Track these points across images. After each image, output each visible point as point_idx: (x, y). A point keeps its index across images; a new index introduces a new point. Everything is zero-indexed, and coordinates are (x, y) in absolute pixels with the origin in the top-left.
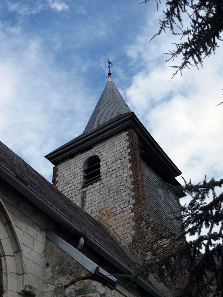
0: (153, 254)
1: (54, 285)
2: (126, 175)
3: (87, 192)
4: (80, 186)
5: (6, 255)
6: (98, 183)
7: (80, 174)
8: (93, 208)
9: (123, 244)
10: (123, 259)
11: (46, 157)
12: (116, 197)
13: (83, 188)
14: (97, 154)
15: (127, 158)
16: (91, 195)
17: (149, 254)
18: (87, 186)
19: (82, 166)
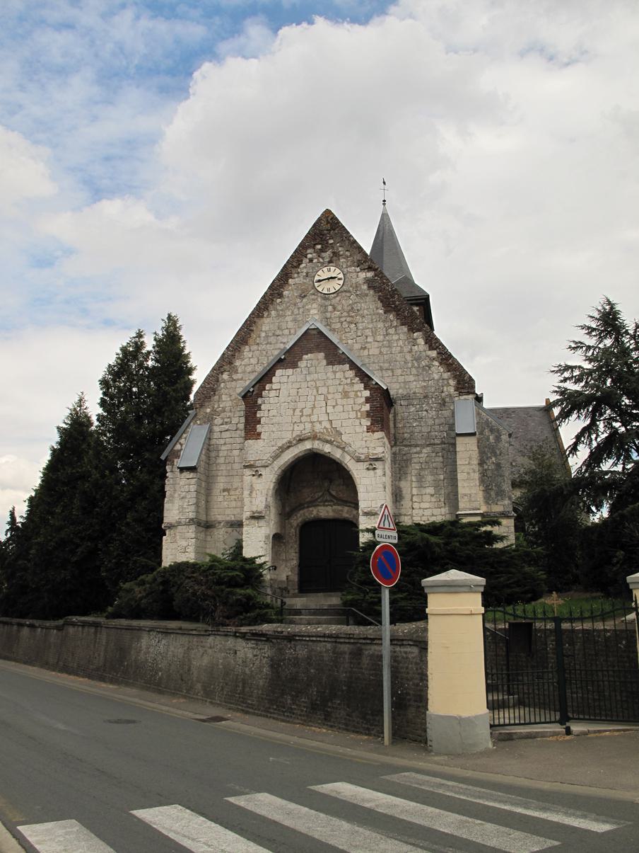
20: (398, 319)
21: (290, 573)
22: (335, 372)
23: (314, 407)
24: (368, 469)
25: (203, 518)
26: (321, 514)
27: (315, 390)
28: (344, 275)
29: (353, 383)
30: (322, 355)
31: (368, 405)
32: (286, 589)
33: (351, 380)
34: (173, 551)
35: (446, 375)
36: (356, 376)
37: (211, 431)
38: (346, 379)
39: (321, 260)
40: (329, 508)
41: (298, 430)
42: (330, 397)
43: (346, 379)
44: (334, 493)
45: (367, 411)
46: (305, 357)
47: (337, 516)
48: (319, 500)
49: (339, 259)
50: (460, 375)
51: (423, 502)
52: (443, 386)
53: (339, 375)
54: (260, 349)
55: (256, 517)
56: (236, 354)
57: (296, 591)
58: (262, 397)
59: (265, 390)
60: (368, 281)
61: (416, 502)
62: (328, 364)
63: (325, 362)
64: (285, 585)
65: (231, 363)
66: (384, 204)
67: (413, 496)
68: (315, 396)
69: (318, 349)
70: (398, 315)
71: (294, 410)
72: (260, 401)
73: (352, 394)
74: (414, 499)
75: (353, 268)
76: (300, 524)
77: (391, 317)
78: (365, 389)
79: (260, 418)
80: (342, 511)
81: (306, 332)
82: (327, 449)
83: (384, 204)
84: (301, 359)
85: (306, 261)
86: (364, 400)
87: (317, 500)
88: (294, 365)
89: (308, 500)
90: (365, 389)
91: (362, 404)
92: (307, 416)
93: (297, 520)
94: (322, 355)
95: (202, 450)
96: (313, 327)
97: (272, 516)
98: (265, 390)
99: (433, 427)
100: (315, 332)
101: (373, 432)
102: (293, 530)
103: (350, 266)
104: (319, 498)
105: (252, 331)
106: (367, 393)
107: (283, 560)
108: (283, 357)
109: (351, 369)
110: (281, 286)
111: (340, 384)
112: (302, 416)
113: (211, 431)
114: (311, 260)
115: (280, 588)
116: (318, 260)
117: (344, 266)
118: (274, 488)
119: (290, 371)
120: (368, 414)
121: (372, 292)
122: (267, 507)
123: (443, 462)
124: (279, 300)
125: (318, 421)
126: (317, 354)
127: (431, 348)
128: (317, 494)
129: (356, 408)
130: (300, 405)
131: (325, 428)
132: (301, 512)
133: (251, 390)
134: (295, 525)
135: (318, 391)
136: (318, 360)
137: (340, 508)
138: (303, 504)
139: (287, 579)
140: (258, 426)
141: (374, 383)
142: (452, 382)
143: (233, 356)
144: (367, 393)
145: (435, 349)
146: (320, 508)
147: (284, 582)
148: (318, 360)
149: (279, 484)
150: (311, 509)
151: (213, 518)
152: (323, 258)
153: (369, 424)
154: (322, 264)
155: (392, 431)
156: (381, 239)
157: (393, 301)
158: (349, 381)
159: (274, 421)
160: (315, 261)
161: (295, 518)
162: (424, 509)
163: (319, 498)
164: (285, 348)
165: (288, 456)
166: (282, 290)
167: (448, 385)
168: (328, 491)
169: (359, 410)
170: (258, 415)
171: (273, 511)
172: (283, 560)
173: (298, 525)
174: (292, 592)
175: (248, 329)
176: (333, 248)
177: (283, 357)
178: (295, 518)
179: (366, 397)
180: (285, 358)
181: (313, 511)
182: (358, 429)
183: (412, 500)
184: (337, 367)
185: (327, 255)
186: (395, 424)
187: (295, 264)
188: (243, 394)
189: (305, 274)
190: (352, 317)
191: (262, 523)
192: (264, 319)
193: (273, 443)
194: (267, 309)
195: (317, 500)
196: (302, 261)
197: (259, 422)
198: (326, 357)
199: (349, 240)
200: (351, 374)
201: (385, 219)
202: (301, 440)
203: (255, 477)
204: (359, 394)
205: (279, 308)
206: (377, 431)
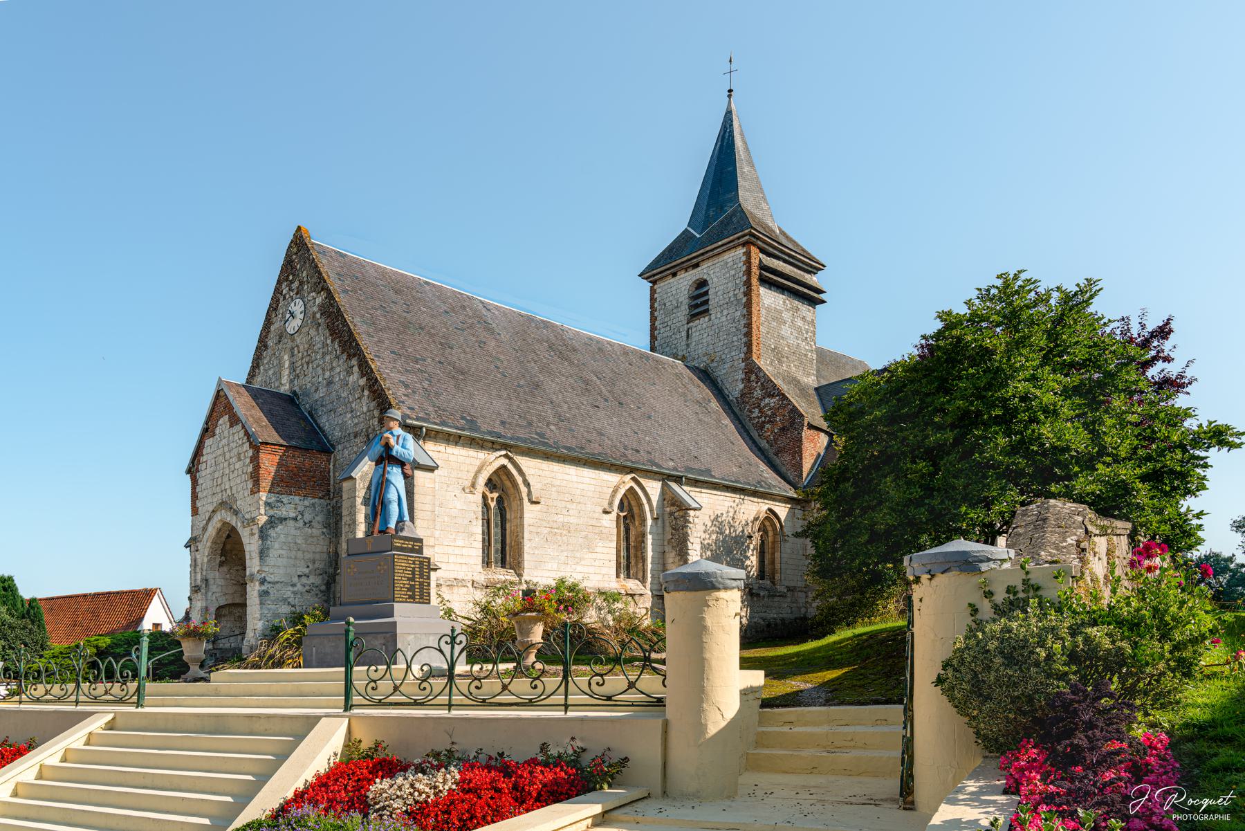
0: (760, 411)
1: (653, 349)
2: (738, 313)
3: (694, 330)
4: (684, 319)
5: (636, 686)
6: (707, 318)
7: (684, 303)
8: (700, 351)
9: (731, 398)
10: (777, 673)
11: (640, 276)
12: (726, 341)
13: (688, 323)
14: (705, 277)
15: (742, 290)
16: (698, 333)
17: (757, 410)
18: (693, 321)
19: (686, 292)
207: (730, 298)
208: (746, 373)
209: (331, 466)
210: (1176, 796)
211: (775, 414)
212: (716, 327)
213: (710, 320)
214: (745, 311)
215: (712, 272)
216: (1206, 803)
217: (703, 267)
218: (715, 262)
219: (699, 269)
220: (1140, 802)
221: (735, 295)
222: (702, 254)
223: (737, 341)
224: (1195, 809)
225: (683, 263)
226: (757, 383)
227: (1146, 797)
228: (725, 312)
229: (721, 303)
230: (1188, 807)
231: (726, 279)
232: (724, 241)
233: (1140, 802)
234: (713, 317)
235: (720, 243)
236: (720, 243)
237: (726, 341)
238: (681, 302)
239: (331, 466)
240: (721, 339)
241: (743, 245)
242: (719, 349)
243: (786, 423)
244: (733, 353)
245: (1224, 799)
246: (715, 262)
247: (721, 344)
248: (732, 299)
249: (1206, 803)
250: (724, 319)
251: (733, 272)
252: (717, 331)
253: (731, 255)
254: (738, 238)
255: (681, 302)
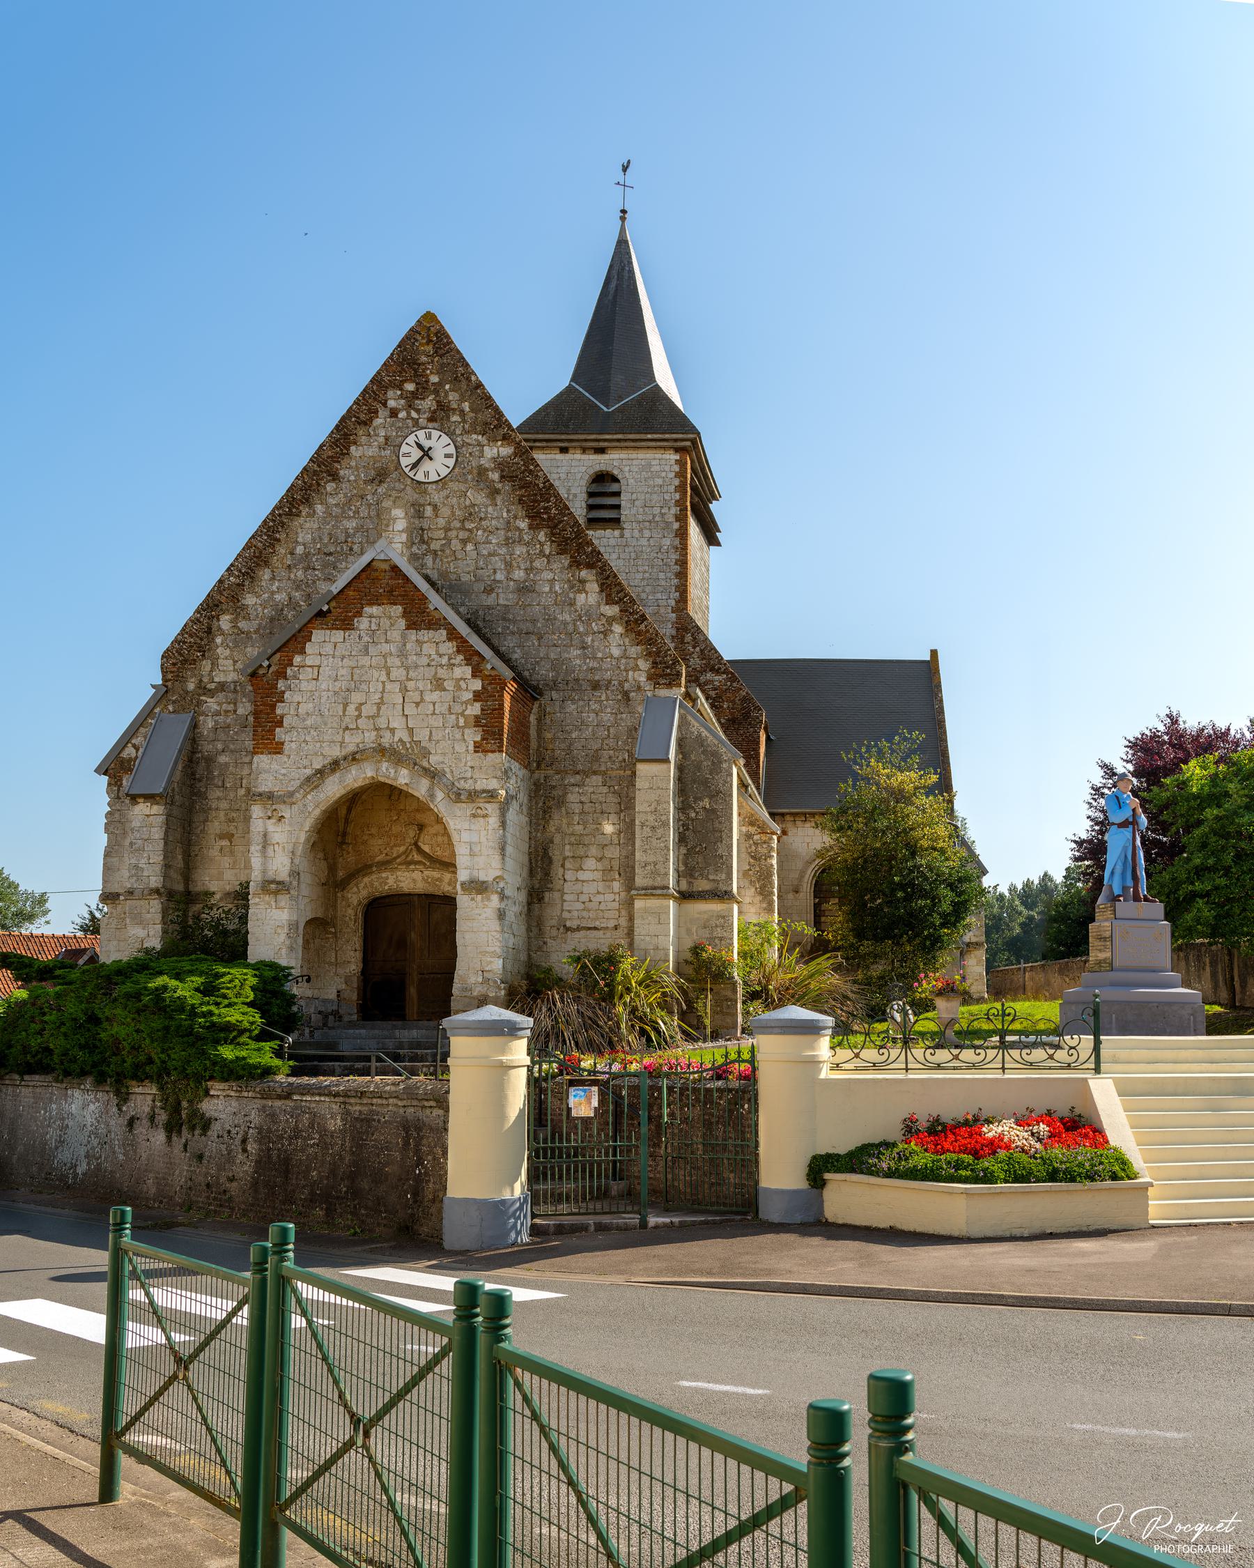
6: (617, 533)
12: (647, 575)
20: (553, 541)
21: (344, 986)
22: (420, 643)
23: (379, 705)
24: (474, 816)
25: (180, 887)
26: (402, 885)
27: (384, 673)
28: (456, 447)
29: (454, 665)
30: (399, 609)
31: (478, 705)
32: (336, 1014)
33: (450, 659)
34: (122, 944)
35: (634, 651)
36: (458, 651)
37: (194, 726)
38: (441, 656)
39: (414, 415)
40: (417, 875)
41: (352, 742)
42: (411, 685)
43: (441, 656)
44: (426, 848)
45: (476, 717)
46: (368, 610)
47: (431, 890)
48: (398, 860)
49: (448, 418)
50: (658, 653)
51: (582, 869)
52: (627, 671)
53: (429, 649)
54: (292, 576)
55: (274, 887)
56: (247, 583)
57: (355, 1017)
58: (285, 678)
59: (292, 665)
60: (500, 464)
61: (569, 870)
62: (408, 628)
63: (402, 623)
64: (330, 1008)
65: (235, 599)
66: (623, 219)
67: (565, 859)
68: (383, 683)
69: (391, 597)
70: (553, 534)
71: (345, 706)
72: (281, 685)
73: (449, 685)
74: (568, 865)
75: (474, 436)
76: (365, 902)
77: (542, 536)
78: (474, 676)
79: (282, 717)
80: (440, 880)
81: (369, 565)
82: (402, 777)
83: (623, 219)
84: (359, 614)
85: (383, 413)
86: (471, 696)
87: (395, 858)
88: (346, 624)
89: (380, 858)
90: (474, 676)
91: (466, 703)
92: (368, 717)
93: (358, 894)
94: (399, 609)
95: (176, 763)
96: (382, 557)
97: (307, 888)
98: (292, 665)
99: (606, 742)
100: (386, 566)
101: (485, 751)
102: (350, 911)
103: (468, 432)
104: (399, 857)
105: (279, 540)
106: (477, 685)
107: (330, 964)
108: (325, 608)
109: (449, 639)
110: (336, 459)
111: (429, 665)
112: (359, 716)
113: (194, 726)
114: (394, 413)
115: (320, 1013)
116: (409, 414)
117: (458, 432)
118: (307, 840)
119: (338, 635)
120: (477, 721)
121: (507, 487)
122: (295, 873)
123: (620, 803)
124: (330, 487)
125: (388, 728)
126: (388, 607)
127: (610, 601)
128: (395, 849)
129: (458, 708)
130: (356, 698)
131: (401, 740)
132: (366, 880)
133: (266, 663)
134: (355, 903)
135: (388, 674)
136: (390, 618)
137: (436, 874)
138: (371, 866)
139: (338, 996)
140: (278, 730)
141: (489, 667)
142: (644, 665)
143: (240, 585)
144: (477, 685)
145: (616, 603)
146: (399, 873)
147: (332, 1001)
148: (390, 618)
149: (319, 832)
150: (384, 875)
151: (198, 888)
152: (418, 411)
153: (478, 738)
154: (416, 422)
155: (534, 744)
156: (610, 297)
157: (545, 508)
158: (444, 660)
159: (308, 722)
160: (402, 415)
161: (355, 889)
162: (583, 881)
163: (399, 857)
164: (330, 591)
165: (334, 789)
166: (336, 465)
167: (636, 668)
168: (416, 844)
169: (462, 714)
170: (278, 711)
171: (306, 878)
172: (330, 964)
173: (360, 903)
174: (346, 1019)
175: (268, 536)
176: (436, 392)
177: (325, 608)
178: (355, 889)
179: (474, 692)
180: (329, 611)
181: (387, 878)
182: (460, 748)
183: (563, 866)
184: (425, 635)
185: (428, 403)
186: (539, 732)
187: (362, 417)
188: (250, 671)
189: (382, 440)
190: (469, 530)
191: (284, 899)
192: (301, 520)
193: (305, 762)
194: (307, 501)
195: (395, 858)
196: (376, 412)
197: (280, 723)
198: (405, 614)
199: (468, 379)
200: (449, 648)
201: (622, 246)
202: (354, 758)
203: (272, 821)
204: (463, 685)
205: (332, 501)
206: (493, 752)
207: (654, 516)
208: (678, 629)
209: (532, 718)
210: (1159, 1519)
211: (720, 697)
212: (631, 549)
213: (622, 536)
214: (677, 541)
215: (627, 469)
216: (1200, 1529)
217: (612, 456)
218: (631, 456)
219: (606, 457)
220: (1108, 1529)
221: (663, 515)
222: (618, 440)
223: (667, 579)
224: (1183, 1539)
225: (586, 440)
226: (694, 647)
227: (1118, 1521)
228: (647, 533)
229: (640, 518)
230: (1176, 1535)
231: (649, 486)
232: (656, 436)
233: (1108, 1529)
234: (627, 533)
235: (649, 436)
236: (649, 436)
237: (647, 575)
238: (575, 496)
239: (532, 718)
240: (640, 569)
241: (677, 450)
242: (636, 582)
243: (737, 715)
244: (659, 596)
245: (1226, 1524)
246: (631, 456)
247: (640, 576)
248: (657, 519)
249: (1200, 1529)
250: (644, 542)
251: (660, 481)
252: (633, 555)
253: (657, 456)
254: (676, 440)
255: (575, 496)
